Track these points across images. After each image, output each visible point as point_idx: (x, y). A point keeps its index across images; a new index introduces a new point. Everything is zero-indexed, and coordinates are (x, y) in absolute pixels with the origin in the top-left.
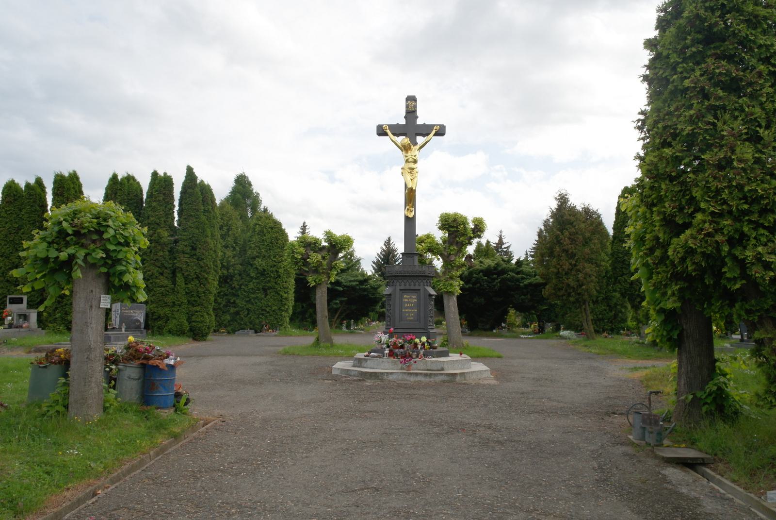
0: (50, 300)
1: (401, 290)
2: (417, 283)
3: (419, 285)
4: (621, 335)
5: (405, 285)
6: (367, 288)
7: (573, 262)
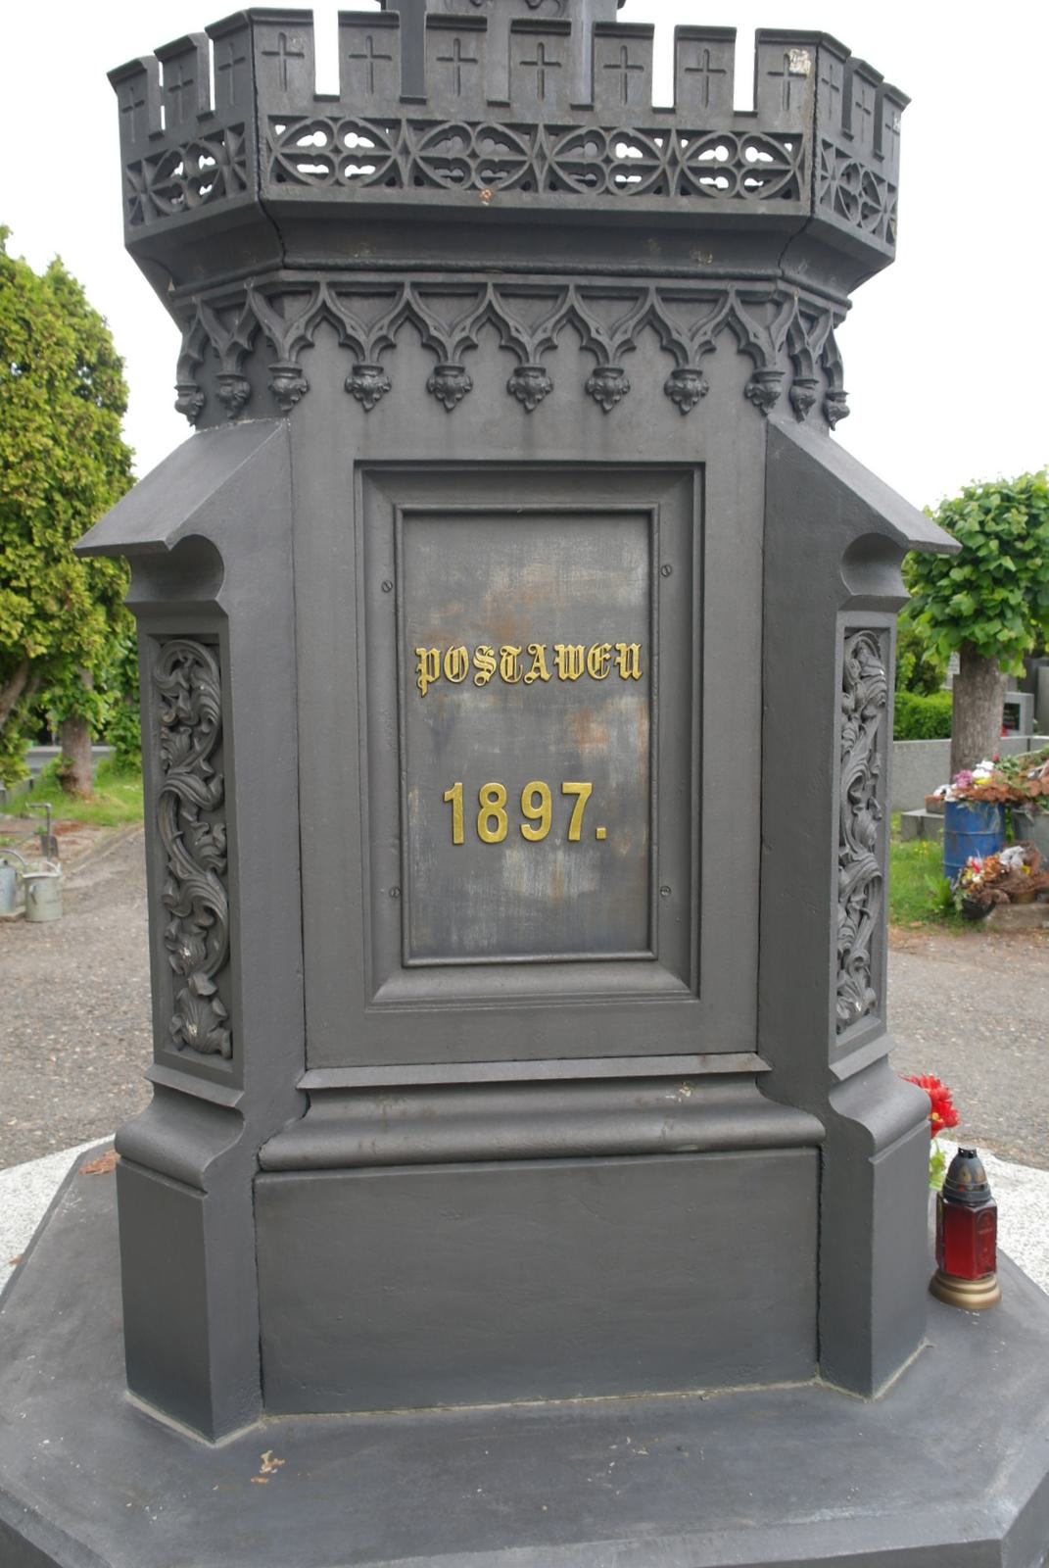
1: (375, 473)
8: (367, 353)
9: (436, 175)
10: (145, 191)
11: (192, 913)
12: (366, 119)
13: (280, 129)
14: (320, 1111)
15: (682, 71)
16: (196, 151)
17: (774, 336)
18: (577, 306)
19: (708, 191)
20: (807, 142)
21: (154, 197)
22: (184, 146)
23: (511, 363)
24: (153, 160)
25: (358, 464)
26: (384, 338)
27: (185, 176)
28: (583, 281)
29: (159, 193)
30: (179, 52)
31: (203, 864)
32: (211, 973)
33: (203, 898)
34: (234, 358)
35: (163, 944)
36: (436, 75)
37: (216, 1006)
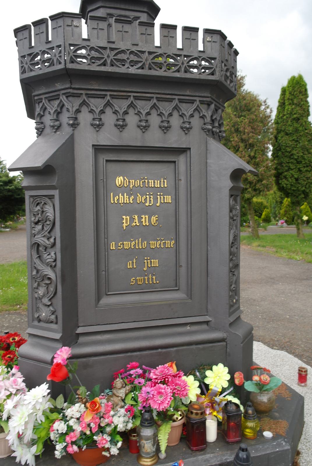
1: (98, 149)
2: (176, 121)
4: (244, 226)
5: (121, 127)
6: (13, 189)
7: (252, 154)
9: (118, 64)
13: (72, 48)
15: (184, 39)
16: (44, 52)
19: (79, 62)
22: (40, 51)
24: (29, 55)
25: (93, 145)
27: (40, 60)
28: (159, 96)
29: (31, 64)
30: (40, 23)
31: (47, 264)
33: (47, 275)
37: (51, 308)
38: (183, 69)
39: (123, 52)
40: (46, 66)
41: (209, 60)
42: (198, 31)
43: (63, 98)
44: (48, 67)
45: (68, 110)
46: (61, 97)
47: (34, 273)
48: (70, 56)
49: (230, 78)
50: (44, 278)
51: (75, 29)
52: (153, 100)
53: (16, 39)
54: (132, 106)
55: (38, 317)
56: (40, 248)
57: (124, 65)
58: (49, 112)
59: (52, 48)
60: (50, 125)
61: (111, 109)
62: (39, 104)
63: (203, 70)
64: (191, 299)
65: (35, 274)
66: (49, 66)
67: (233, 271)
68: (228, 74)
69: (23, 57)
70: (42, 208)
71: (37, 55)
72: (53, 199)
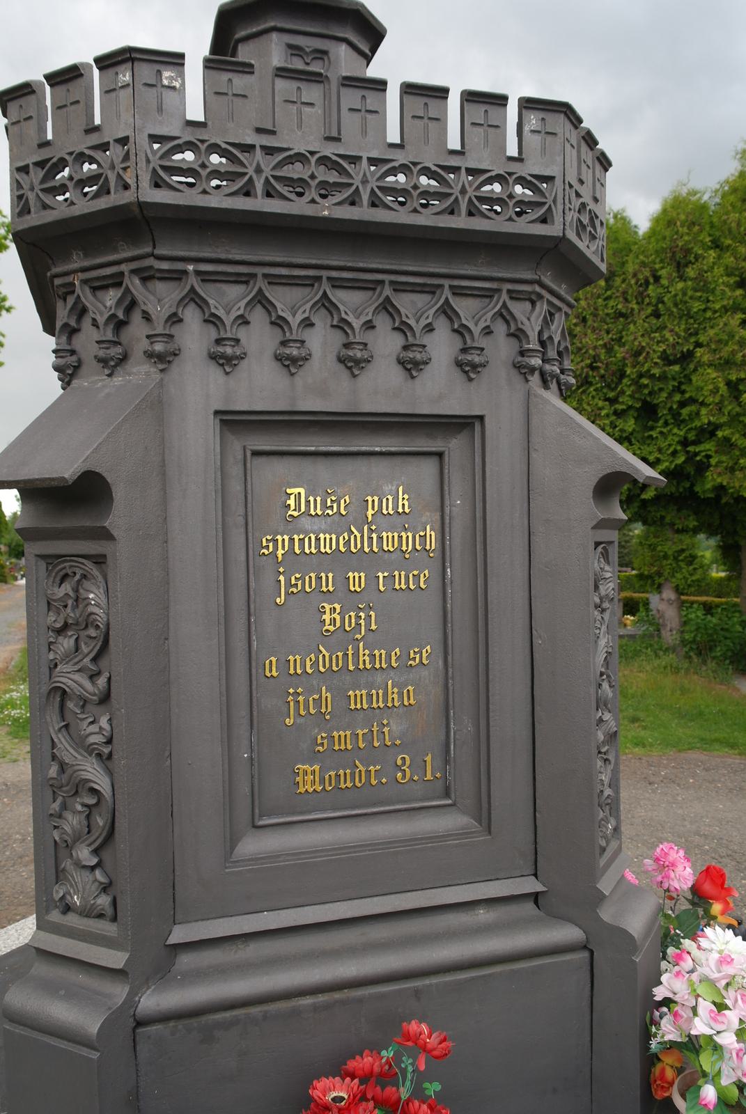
0: (365, 192)
1: (233, 422)
3: (468, 368)
5: (411, 366)
8: (228, 328)
10: (32, 189)
11: (76, 793)
12: (337, 155)
13: (156, 146)
14: (186, 961)
16: (81, 158)
17: (533, 324)
18: (264, 288)
20: (558, 181)
21: (39, 193)
22: (71, 154)
23: (277, 335)
24: (40, 164)
25: (217, 413)
26: (241, 316)
27: (71, 178)
30: (67, 77)
31: (90, 750)
32: (93, 847)
34: (112, 326)
35: (45, 820)
36: (350, 124)
38: (365, 197)
39: (300, 158)
40: (85, 194)
41: (442, 173)
42: (385, 90)
43: (135, 284)
44: (93, 198)
45: (147, 317)
46: (126, 281)
47: (53, 771)
48: (151, 166)
49: (589, 229)
50: (80, 790)
51: (169, 97)
52: (255, 284)
53: (5, 121)
54: (323, 305)
55: (63, 898)
56: (70, 705)
57: (300, 195)
58: (94, 320)
59: (104, 147)
60: (96, 357)
61: (198, 311)
62: (65, 300)
63: (215, 183)
64: (490, 833)
65: (54, 775)
66: (97, 195)
67: (603, 750)
68: (586, 220)
69: (24, 170)
70: (76, 591)
71: (62, 164)
72: (103, 565)
